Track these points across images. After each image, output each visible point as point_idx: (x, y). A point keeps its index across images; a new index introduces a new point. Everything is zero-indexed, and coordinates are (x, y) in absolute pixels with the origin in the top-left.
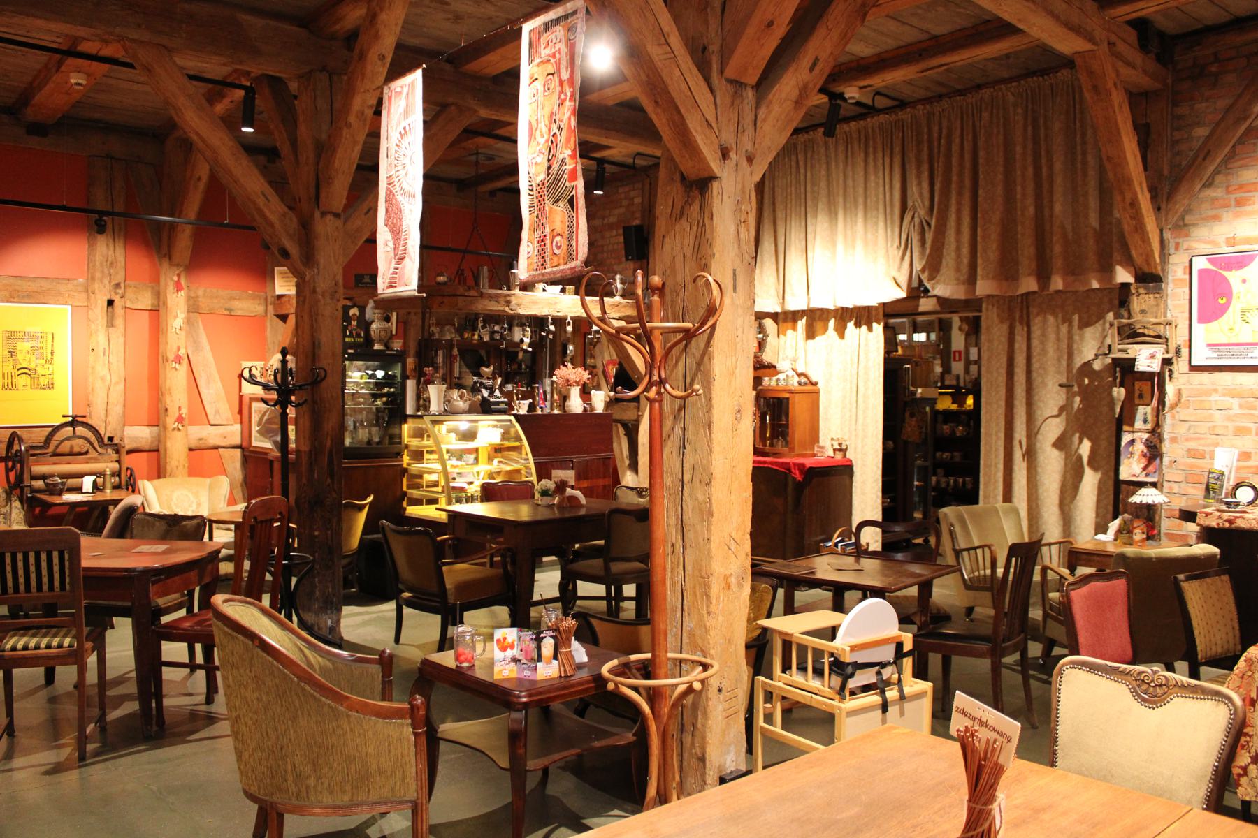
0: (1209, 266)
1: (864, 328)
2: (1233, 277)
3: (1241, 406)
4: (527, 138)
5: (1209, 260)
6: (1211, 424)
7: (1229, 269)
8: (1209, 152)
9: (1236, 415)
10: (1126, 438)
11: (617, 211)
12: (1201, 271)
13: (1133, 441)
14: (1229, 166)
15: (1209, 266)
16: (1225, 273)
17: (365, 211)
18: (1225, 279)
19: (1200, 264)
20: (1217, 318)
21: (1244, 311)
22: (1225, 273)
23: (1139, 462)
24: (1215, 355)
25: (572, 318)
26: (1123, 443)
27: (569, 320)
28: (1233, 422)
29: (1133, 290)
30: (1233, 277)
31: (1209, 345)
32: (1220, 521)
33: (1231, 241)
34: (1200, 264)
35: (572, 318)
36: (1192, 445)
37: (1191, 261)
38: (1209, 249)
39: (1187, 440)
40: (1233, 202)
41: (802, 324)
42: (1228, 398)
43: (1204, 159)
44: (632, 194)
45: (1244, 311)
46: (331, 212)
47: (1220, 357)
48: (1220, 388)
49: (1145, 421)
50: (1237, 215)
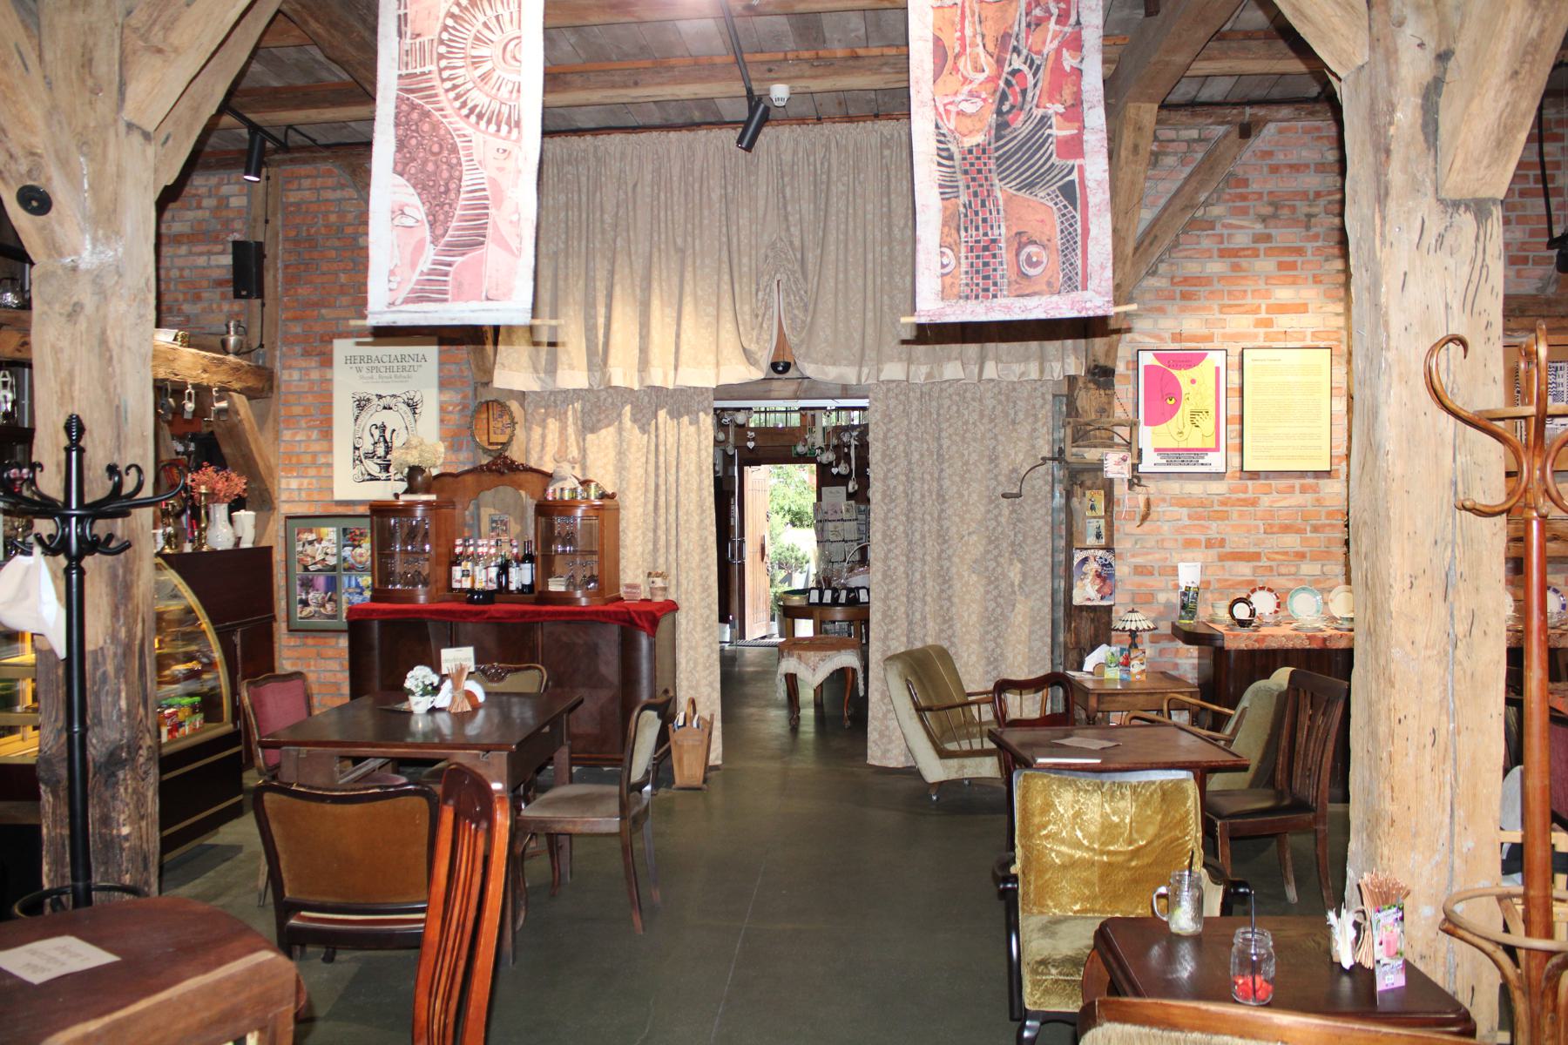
0: (1156, 363)
1: (685, 419)
2: (1182, 376)
3: (1190, 517)
4: (929, 65)
5: (1156, 356)
6: (1159, 537)
7: (1178, 367)
8: (1156, 237)
9: (1186, 527)
10: (1078, 556)
11: (190, 215)
12: (1148, 368)
13: (1085, 560)
14: (1173, 255)
15: (1156, 363)
16: (1175, 372)
17: (163, 139)
18: (1174, 378)
19: (1147, 359)
20: (1165, 421)
21: (1194, 414)
22: (1175, 372)
23: (1093, 583)
24: (1164, 461)
25: (195, 386)
26: (1076, 562)
27: (190, 390)
28: (1182, 533)
29: (1081, 384)
30: (1182, 376)
31: (1157, 450)
32: (1248, 642)
33: (1178, 337)
34: (1147, 359)
35: (195, 386)
36: (1139, 560)
37: (1242, 354)
38: (1154, 343)
39: (1133, 556)
40: (1178, 295)
41: (573, 411)
42: (1176, 509)
43: (1151, 244)
44: (225, 190)
45: (1194, 414)
46: (138, 128)
47: (1169, 463)
48: (1168, 497)
49: (1098, 536)
50: (1183, 310)
